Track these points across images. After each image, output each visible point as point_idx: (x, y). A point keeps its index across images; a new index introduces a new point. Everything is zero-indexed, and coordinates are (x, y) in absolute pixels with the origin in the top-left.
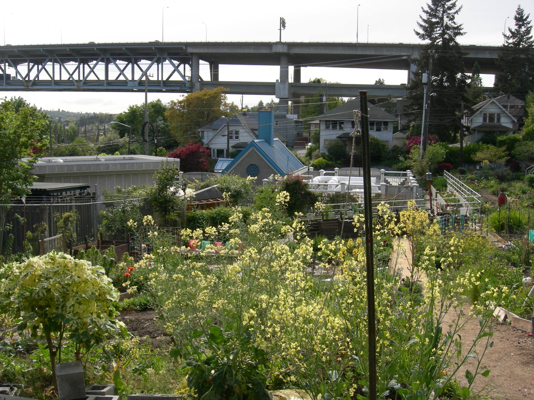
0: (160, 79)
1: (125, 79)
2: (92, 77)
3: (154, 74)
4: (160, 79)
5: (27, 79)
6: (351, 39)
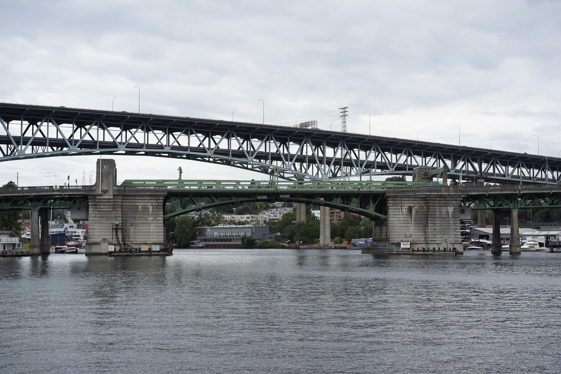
0: (268, 151)
1: (42, 136)
2: (87, 138)
3: (224, 145)
4: (268, 151)
5: (119, 140)
6: (110, 110)
